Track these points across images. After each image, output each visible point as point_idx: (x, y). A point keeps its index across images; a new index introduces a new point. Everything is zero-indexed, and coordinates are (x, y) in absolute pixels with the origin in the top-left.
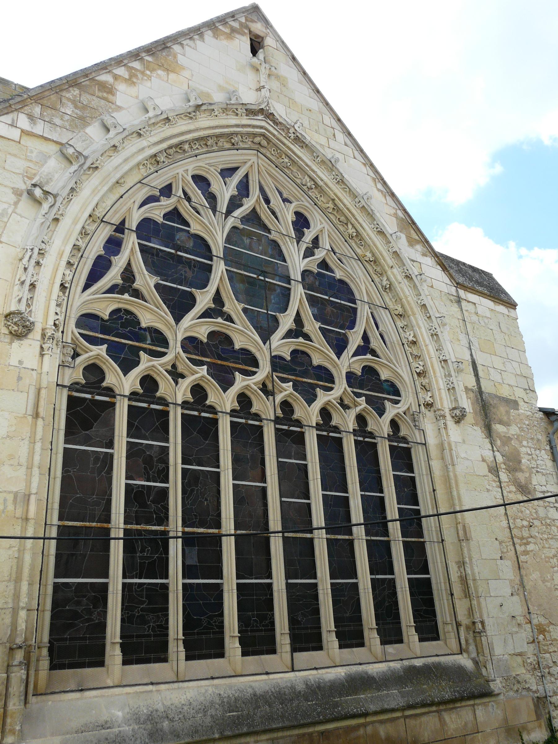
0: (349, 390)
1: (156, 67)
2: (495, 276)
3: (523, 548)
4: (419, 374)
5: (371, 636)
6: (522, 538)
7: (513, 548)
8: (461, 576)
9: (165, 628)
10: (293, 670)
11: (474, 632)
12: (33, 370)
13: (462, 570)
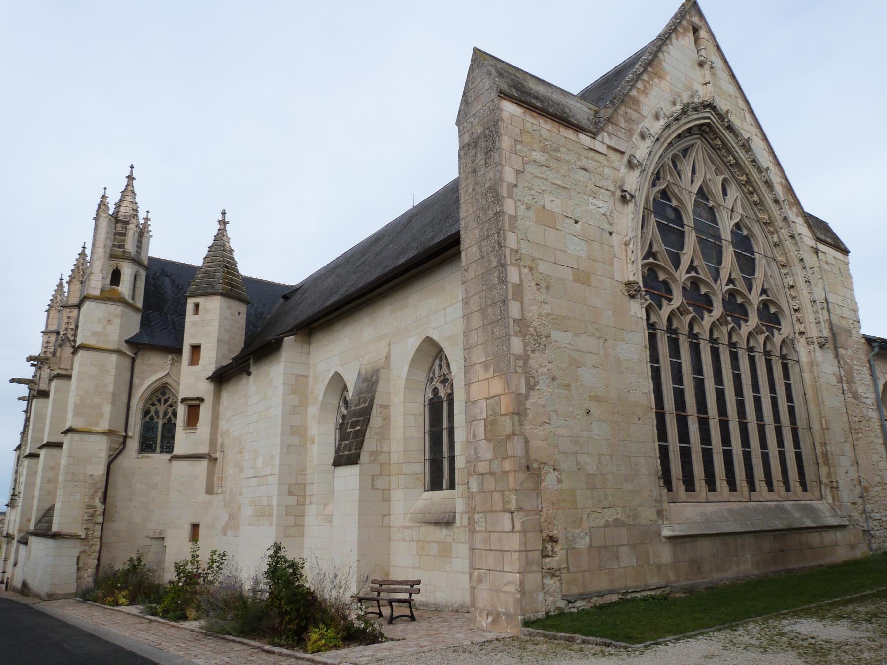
2: (831, 225)
4: (796, 311)
6: (856, 430)
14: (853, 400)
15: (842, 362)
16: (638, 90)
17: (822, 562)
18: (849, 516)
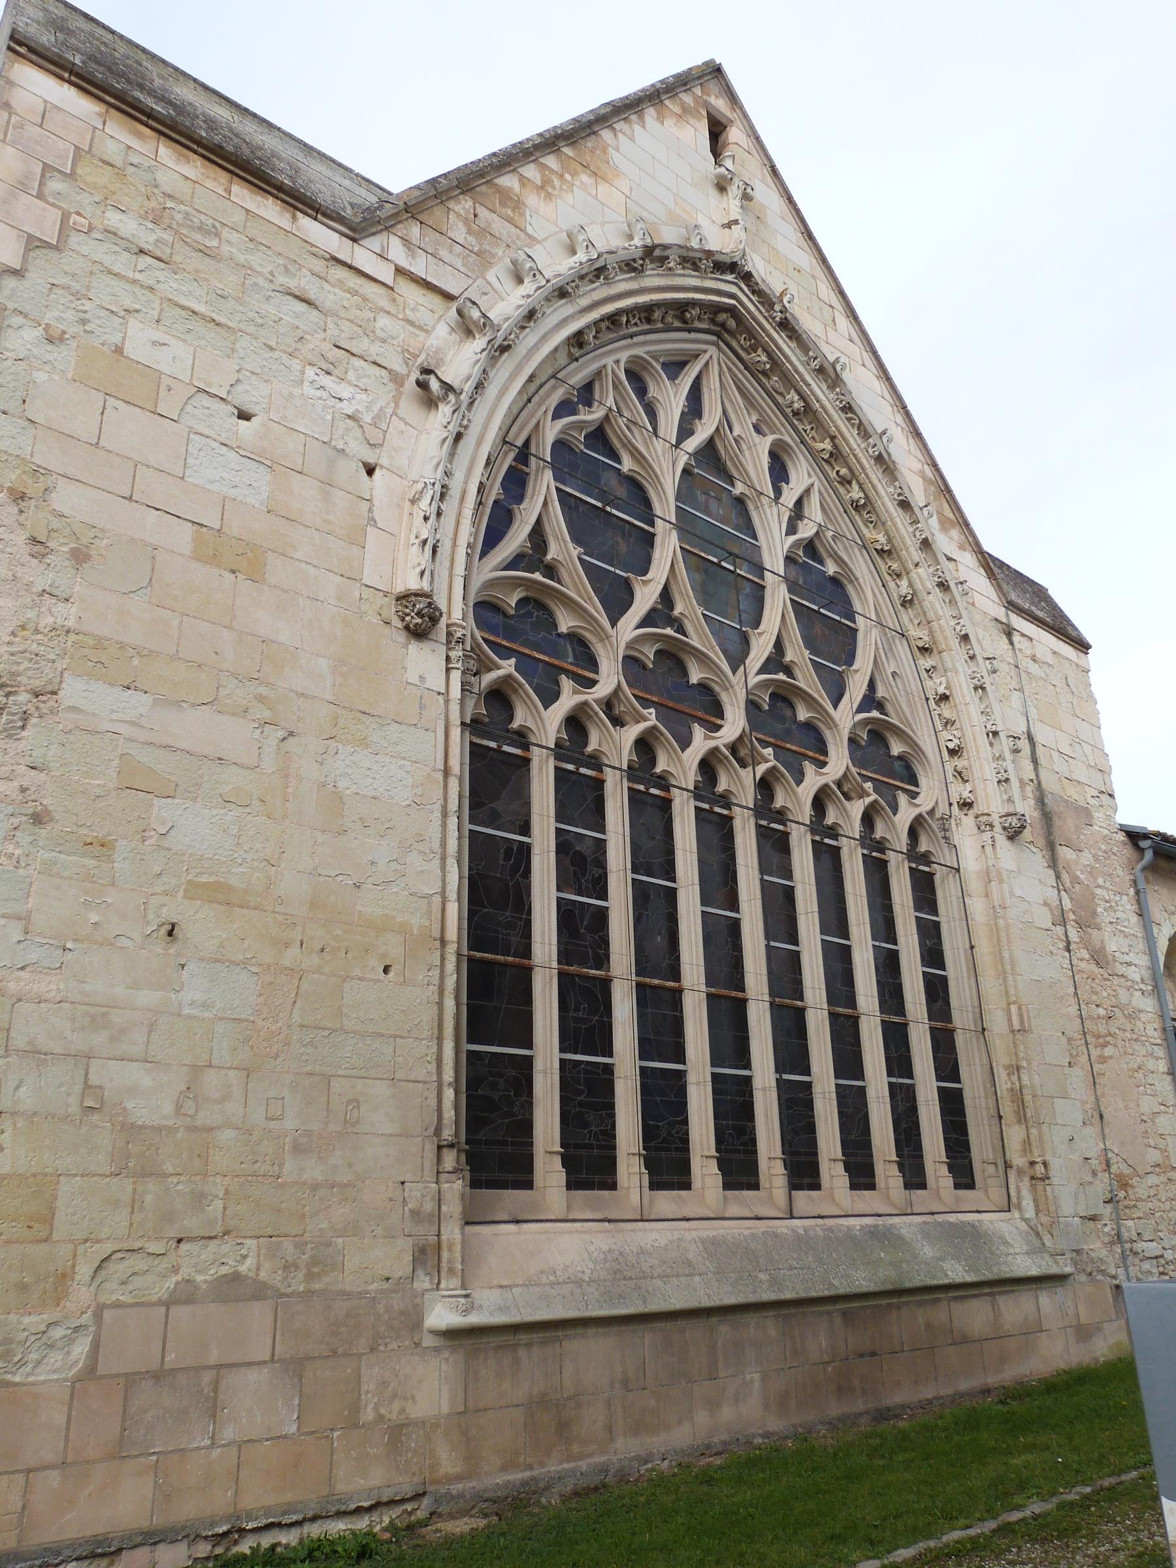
0: (854, 770)
1: (579, 167)
3: (1098, 1051)
4: (953, 752)
5: (833, 1173)
6: (1098, 1036)
7: (1085, 1051)
8: (1012, 1090)
9: (609, 1135)
10: (792, 1217)
11: (1032, 1178)
12: (439, 693)
13: (1015, 1078)
14: (1093, 967)
15: (1065, 877)
16: (523, 181)
17: (992, 1380)
18: (1078, 1252)
